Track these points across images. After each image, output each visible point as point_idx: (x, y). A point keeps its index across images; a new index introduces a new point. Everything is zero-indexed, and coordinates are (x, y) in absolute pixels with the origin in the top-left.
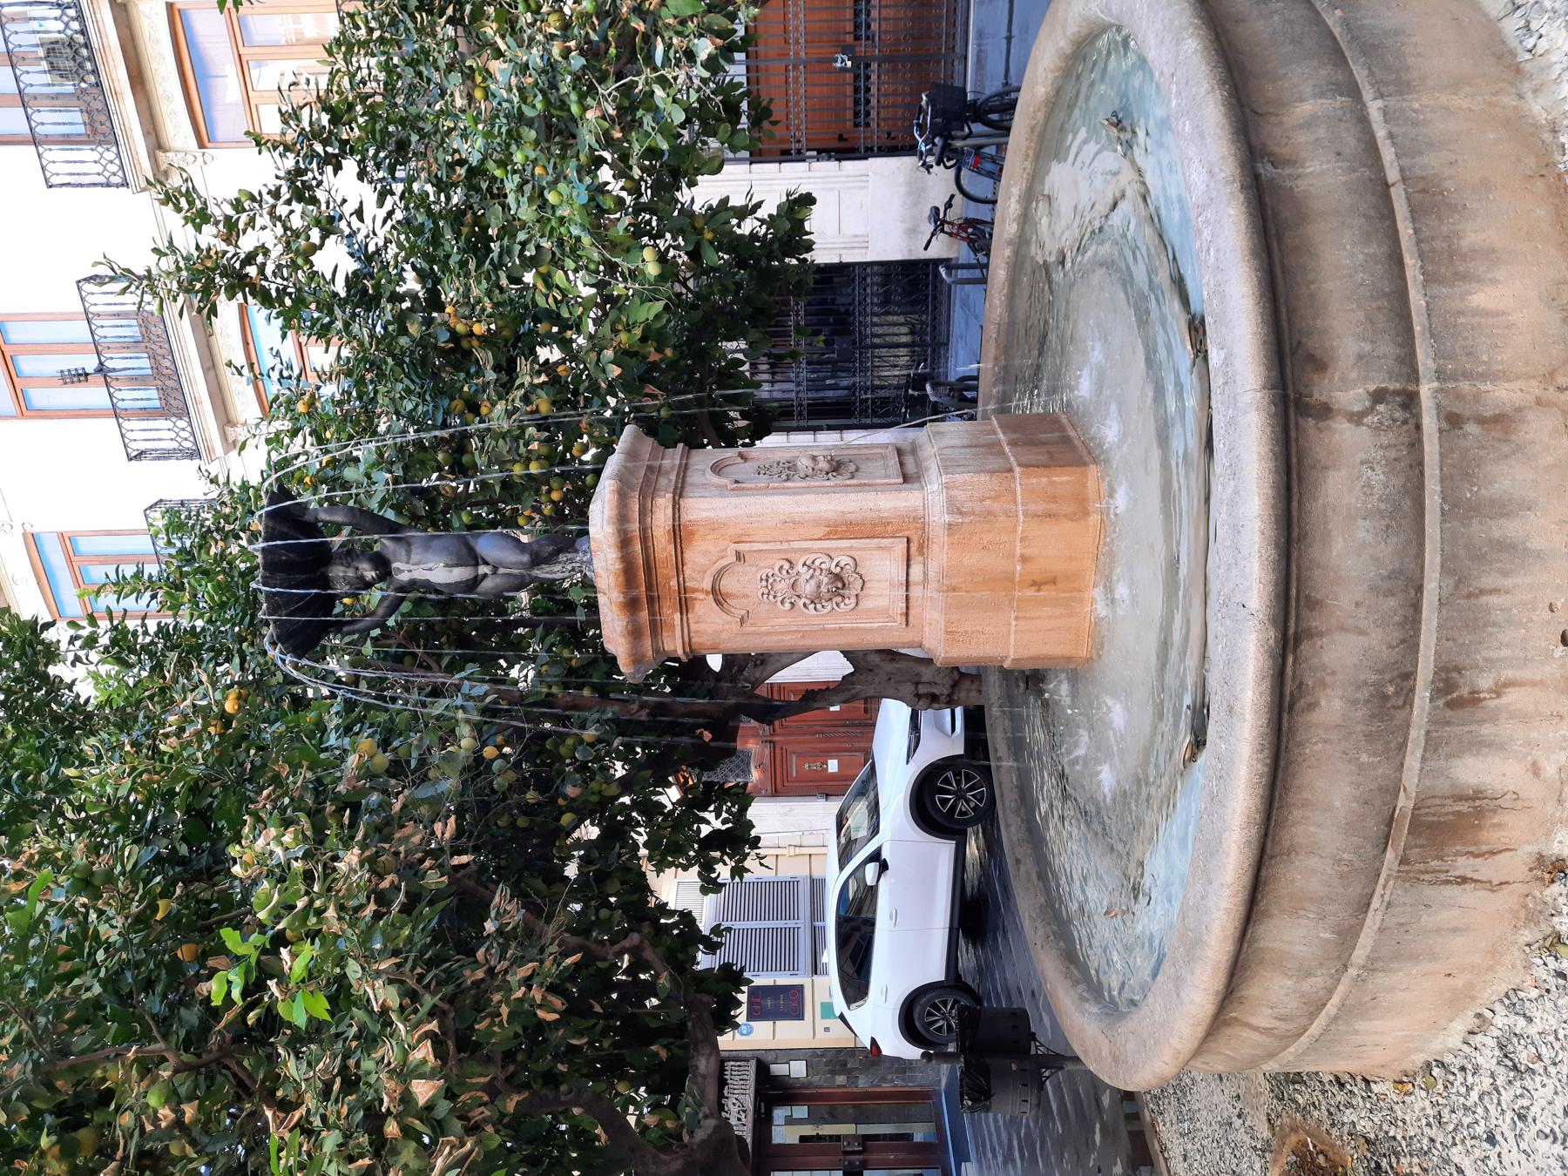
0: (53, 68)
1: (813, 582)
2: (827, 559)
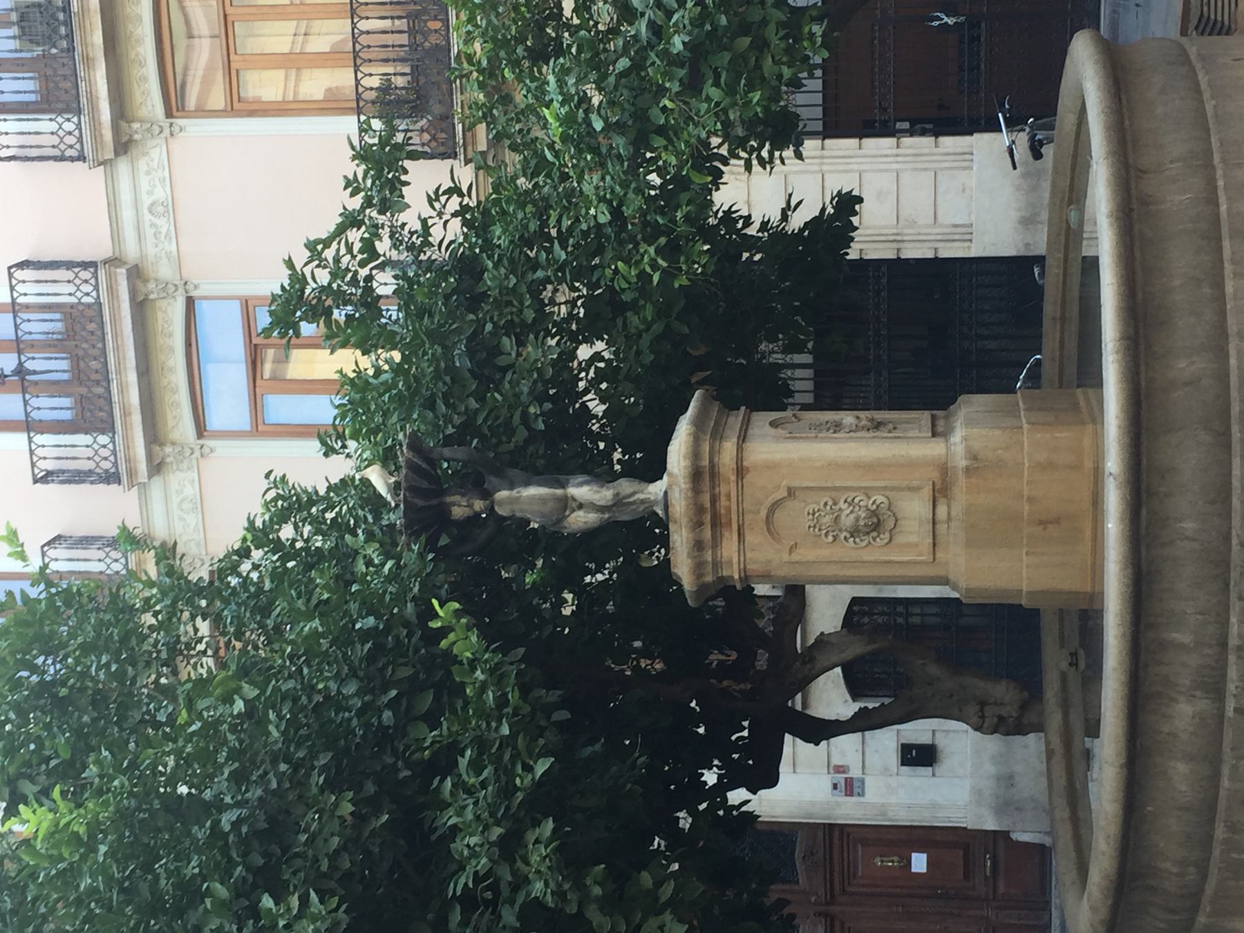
1: (852, 516)
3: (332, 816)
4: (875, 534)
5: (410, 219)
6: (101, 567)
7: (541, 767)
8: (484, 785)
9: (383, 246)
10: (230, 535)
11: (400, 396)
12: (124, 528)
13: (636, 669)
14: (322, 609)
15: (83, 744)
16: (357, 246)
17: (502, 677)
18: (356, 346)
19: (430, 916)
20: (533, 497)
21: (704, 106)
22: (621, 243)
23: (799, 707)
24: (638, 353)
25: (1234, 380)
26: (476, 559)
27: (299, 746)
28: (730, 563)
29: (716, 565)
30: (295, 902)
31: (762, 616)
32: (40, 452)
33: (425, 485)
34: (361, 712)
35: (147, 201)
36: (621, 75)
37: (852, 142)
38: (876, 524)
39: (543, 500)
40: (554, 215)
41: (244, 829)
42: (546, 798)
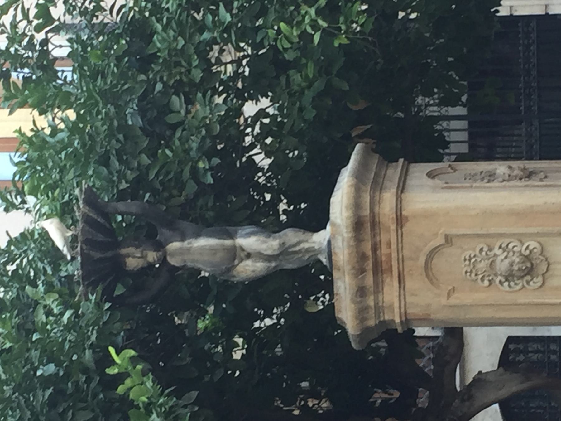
1: (507, 261)
2: (518, 244)
4: (528, 278)
11: (75, 155)
13: (304, 408)
20: (202, 248)
26: (150, 307)
28: (391, 307)
29: (379, 309)
31: (422, 356)
33: (100, 237)
39: (213, 250)
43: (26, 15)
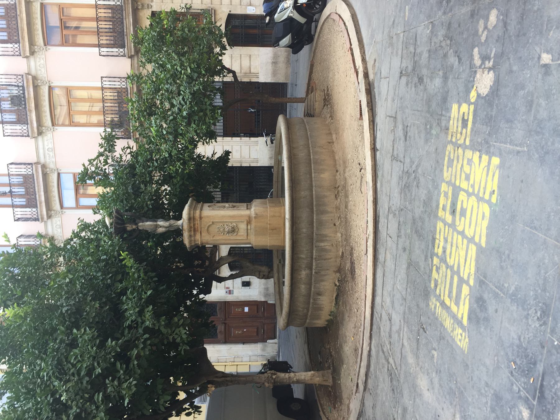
0: (12, 103)
3: (93, 307)
5: (117, 154)
6: (34, 243)
7: (149, 293)
8: (134, 298)
9: (110, 161)
10: (68, 235)
11: (114, 199)
12: (39, 233)
13: (177, 266)
14: (92, 254)
15: (24, 291)
16: (102, 161)
17: (139, 271)
18: (102, 186)
19: (120, 332)
20: (148, 225)
21: (191, 129)
22: (171, 162)
23: (218, 274)
24: (176, 189)
25: (314, 196)
26: (134, 241)
27: (85, 289)
28: (198, 240)
29: (195, 241)
30: (83, 330)
31: (207, 252)
32: (16, 213)
33: (120, 222)
34: (102, 280)
35: (47, 148)
36: (171, 121)
37: (230, 138)
38: (233, 230)
39: (151, 225)
40: (154, 155)
41: (69, 312)
42: (150, 301)
43: (100, 162)
